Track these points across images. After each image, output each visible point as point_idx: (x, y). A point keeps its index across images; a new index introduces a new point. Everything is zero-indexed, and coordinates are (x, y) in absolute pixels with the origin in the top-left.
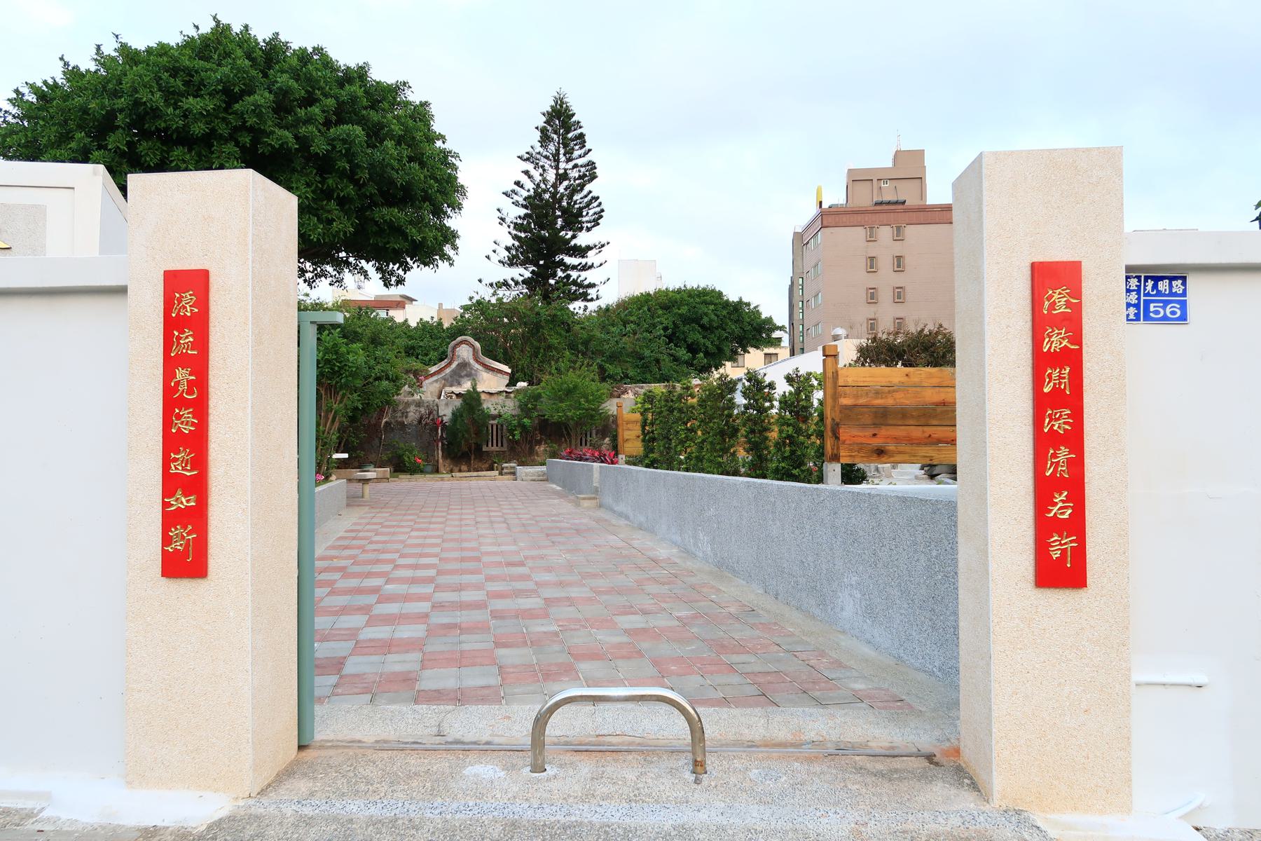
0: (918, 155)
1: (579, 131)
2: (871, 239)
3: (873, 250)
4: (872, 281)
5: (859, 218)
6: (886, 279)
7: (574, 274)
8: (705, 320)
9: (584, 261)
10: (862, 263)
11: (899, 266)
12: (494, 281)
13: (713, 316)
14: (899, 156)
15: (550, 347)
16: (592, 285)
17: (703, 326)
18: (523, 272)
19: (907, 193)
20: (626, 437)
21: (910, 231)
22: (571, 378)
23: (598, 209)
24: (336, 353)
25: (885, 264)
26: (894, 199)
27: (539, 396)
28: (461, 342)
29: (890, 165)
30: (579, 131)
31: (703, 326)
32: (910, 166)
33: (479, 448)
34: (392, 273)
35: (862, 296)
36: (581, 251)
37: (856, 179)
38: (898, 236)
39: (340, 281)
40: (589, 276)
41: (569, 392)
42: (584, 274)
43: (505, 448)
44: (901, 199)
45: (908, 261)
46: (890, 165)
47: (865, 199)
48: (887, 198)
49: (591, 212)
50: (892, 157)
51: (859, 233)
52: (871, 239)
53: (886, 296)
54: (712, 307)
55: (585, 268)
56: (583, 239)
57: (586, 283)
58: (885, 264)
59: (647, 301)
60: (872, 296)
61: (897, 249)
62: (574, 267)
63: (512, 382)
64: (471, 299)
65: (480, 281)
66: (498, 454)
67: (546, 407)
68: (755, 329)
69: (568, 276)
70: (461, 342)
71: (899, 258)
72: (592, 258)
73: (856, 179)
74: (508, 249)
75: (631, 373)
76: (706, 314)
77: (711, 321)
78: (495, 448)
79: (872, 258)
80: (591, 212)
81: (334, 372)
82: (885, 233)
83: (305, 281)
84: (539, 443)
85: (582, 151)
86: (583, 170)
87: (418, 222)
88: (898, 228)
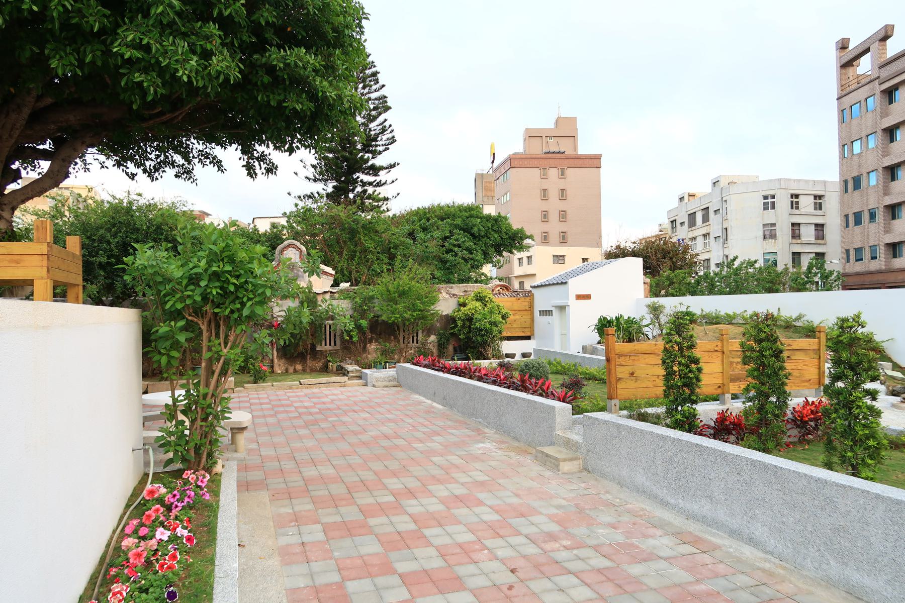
0: (573, 120)
1: (374, 70)
2: (544, 177)
3: (545, 185)
4: (544, 206)
5: (536, 162)
6: (554, 205)
7: (370, 190)
8: (475, 230)
9: (378, 179)
10: (538, 193)
11: (544, 196)
12: (397, 167)
13: (481, 228)
14: (559, 121)
15: (365, 251)
16: (386, 199)
17: (473, 235)
18: (330, 187)
19: (565, 146)
20: (619, 375)
21: (570, 172)
22: (404, 279)
23: (390, 135)
24: (232, 261)
25: (553, 194)
26: (557, 150)
27: (372, 298)
28: (289, 246)
29: (553, 127)
30: (374, 70)
31: (473, 235)
32: (566, 129)
33: (313, 347)
34: (262, 158)
35: (539, 216)
36: (375, 170)
37: (531, 136)
38: (562, 175)
39: (188, 172)
40: (383, 192)
41: (403, 294)
42: (378, 189)
43: (338, 347)
44: (562, 150)
45: (568, 192)
46: (553, 127)
47: (537, 149)
48: (552, 150)
49: (385, 138)
50: (554, 121)
51: (536, 172)
52: (544, 177)
53: (554, 217)
54: (479, 220)
55: (379, 184)
56: (379, 161)
57: (381, 196)
58: (553, 194)
59: (425, 214)
60: (545, 216)
61: (562, 184)
62: (370, 184)
63: (336, 284)
64: (296, 205)
65: (289, 194)
66: (333, 353)
67: (378, 307)
68: (510, 237)
69: (365, 191)
70: (289, 246)
71: (563, 190)
72: (383, 176)
73: (531, 136)
74: (314, 166)
75: (437, 274)
76: (474, 226)
77: (479, 230)
78: (328, 347)
79: (545, 190)
80: (385, 138)
81: (225, 294)
82: (553, 173)
83: (145, 171)
84: (371, 342)
85: (378, 86)
86: (377, 102)
87: (329, 70)
88: (562, 170)
